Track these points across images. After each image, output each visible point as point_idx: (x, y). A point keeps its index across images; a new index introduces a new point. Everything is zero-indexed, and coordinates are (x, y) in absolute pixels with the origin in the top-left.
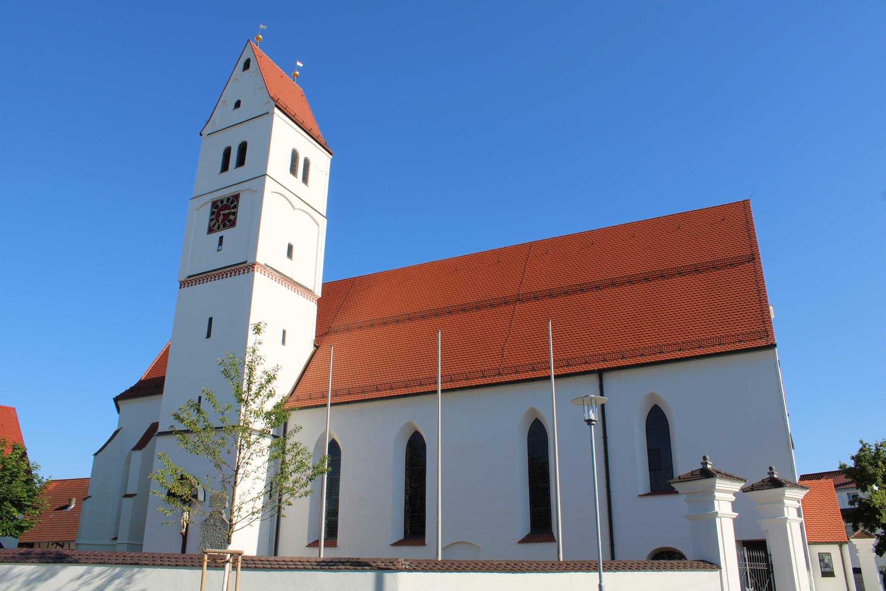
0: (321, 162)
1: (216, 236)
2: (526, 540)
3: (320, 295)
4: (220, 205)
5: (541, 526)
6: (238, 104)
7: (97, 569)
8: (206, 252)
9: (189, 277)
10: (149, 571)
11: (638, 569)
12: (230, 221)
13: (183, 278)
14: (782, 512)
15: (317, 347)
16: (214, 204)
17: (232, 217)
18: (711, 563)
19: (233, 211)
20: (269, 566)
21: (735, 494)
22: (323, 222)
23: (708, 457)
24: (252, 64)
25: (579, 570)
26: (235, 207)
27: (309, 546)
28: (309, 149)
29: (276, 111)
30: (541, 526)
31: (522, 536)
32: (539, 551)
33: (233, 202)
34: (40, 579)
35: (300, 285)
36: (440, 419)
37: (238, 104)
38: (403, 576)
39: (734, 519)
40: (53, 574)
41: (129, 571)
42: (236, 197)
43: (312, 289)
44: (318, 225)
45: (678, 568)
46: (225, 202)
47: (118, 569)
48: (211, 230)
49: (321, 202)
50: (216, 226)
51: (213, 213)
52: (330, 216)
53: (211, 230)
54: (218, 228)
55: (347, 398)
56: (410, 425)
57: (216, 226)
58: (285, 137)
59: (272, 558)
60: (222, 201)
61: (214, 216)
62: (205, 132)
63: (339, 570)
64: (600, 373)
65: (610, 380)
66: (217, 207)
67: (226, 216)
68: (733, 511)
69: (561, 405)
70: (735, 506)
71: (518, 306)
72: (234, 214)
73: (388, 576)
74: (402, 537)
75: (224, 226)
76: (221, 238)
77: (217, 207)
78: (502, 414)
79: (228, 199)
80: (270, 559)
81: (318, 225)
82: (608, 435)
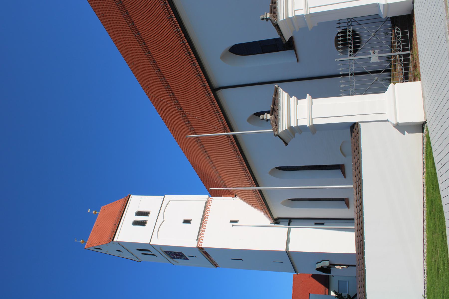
0: (137, 202)
14: (302, 16)
20: (362, 248)
22: (168, 197)
23: (261, 17)
27: (348, 207)
28: (129, 216)
29: (115, 240)
32: (349, 170)
35: (204, 213)
39: (313, 97)
43: (205, 202)
44: (170, 201)
49: (158, 199)
52: (163, 193)
59: (356, 221)
64: (215, 90)
65: (218, 81)
68: (305, 98)
81: (170, 201)
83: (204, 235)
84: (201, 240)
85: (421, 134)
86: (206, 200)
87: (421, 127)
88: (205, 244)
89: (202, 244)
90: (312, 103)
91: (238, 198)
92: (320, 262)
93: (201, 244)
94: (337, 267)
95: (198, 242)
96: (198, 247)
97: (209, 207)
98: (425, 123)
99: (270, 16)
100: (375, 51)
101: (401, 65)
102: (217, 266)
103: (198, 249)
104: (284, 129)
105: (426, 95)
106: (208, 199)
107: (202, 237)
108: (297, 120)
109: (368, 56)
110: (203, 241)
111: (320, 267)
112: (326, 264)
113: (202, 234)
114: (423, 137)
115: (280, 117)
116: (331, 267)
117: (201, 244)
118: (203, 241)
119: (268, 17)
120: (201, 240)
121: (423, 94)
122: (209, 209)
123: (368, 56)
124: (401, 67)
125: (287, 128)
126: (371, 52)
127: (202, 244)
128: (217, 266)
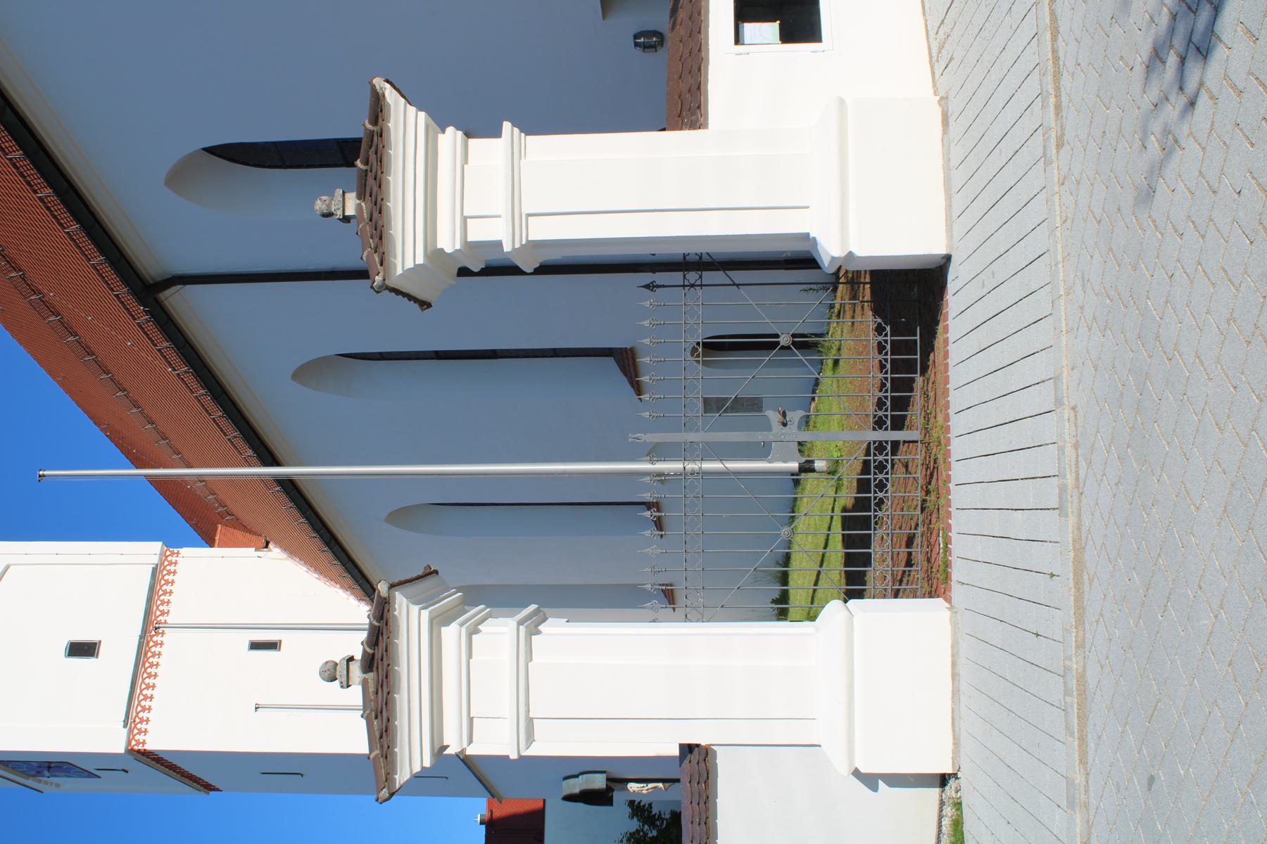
23: (320, 206)
35: (148, 612)
44: (8, 567)
81: (8, 567)
83: (151, 715)
84: (142, 721)
85: (938, 790)
86: (156, 560)
87: (943, 780)
88: (156, 740)
89: (147, 738)
90: (529, 656)
91: (275, 552)
92: (576, 776)
93: (140, 737)
94: (633, 787)
95: (131, 731)
96: (130, 751)
97: (168, 588)
98: (948, 258)
99: (359, 208)
100: (789, 415)
101: (882, 367)
102: (208, 787)
103: (131, 758)
104: (417, 769)
105: (955, 106)
106: (163, 556)
107: (144, 709)
108: (471, 720)
109: (760, 437)
110: (149, 727)
111: (577, 791)
112: (599, 782)
113: (146, 697)
114: (942, 803)
115: (402, 669)
116: (613, 790)
117: (140, 737)
118: (149, 727)
119: (350, 211)
120: (142, 721)
121: (954, 664)
122: (166, 598)
123: (760, 437)
124: (881, 376)
125: (427, 764)
126: (773, 416)
127: (147, 738)
128: (208, 787)
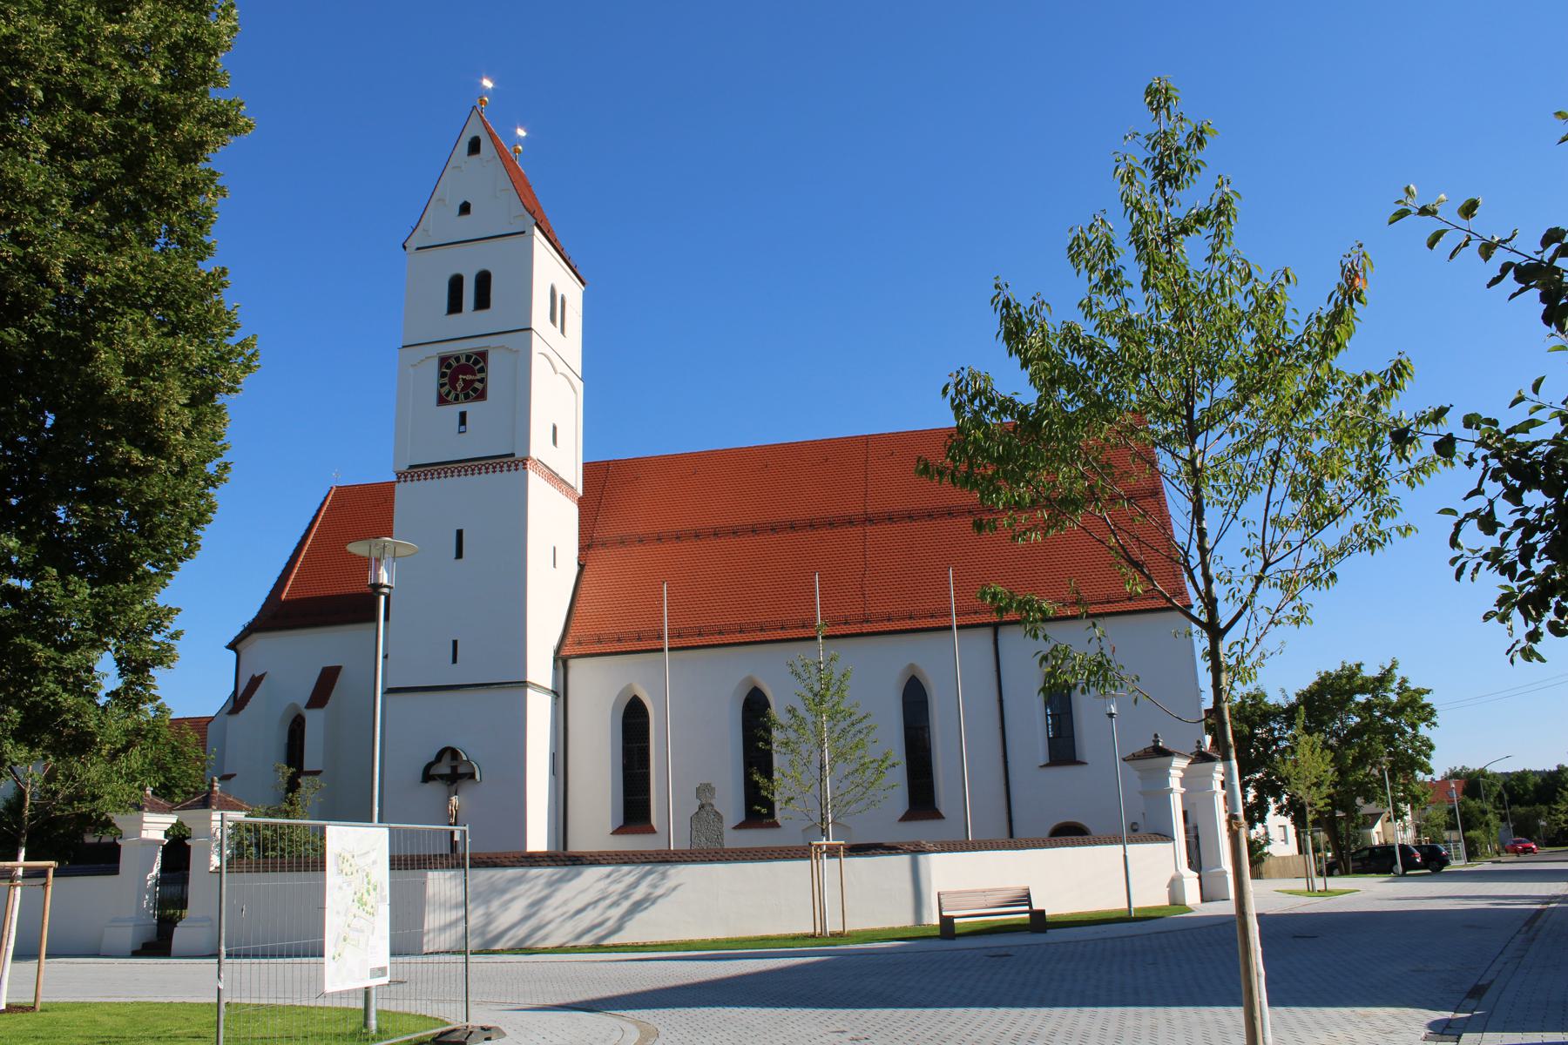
1: (454, 410)
2: (907, 817)
3: (580, 492)
4: (455, 364)
5: (922, 799)
6: (465, 209)
7: (626, 868)
8: (440, 434)
9: (411, 467)
10: (682, 867)
11: (998, 848)
12: (475, 390)
13: (404, 468)
15: (582, 567)
16: (444, 361)
17: (478, 385)
18: (1167, 837)
19: (479, 376)
21: (1183, 770)
22: (580, 385)
24: (486, 144)
25: (777, 859)
26: (482, 370)
30: (922, 799)
31: (901, 813)
33: (476, 362)
34: (562, 880)
36: (779, 673)
37: (465, 209)
38: (934, 857)
40: (578, 875)
41: (661, 868)
42: (483, 355)
45: (1085, 844)
46: (463, 361)
47: (648, 867)
48: (442, 400)
50: (452, 395)
51: (443, 375)
53: (442, 400)
54: (457, 398)
55: (635, 642)
56: (749, 679)
57: (452, 395)
58: (548, 270)
60: (457, 359)
61: (446, 380)
62: (414, 242)
63: (874, 855)
64: (996, 627)
66: (449, 366)
67: (468, 384)
69: (955, 667)
70: (1183, 782)
71: (869, 528)
72: (482, 381)
73: (922, 858)
74: (743, 818)
75: (467, 397)
76: (463, 416)
77: (449, 366)
78: (871, 674)
79: (468, 357)
80: (563, 857)
82: (1005, 697)
